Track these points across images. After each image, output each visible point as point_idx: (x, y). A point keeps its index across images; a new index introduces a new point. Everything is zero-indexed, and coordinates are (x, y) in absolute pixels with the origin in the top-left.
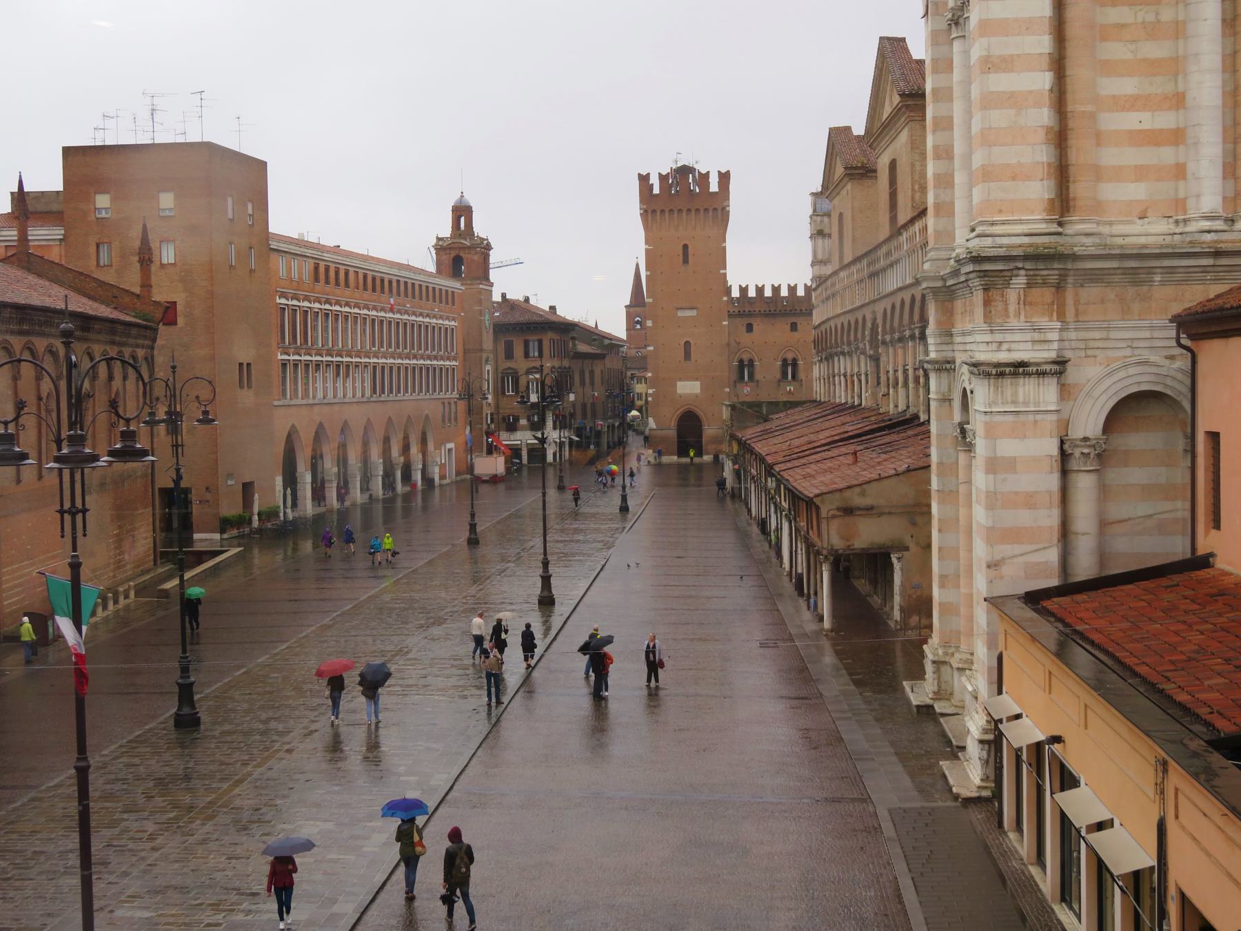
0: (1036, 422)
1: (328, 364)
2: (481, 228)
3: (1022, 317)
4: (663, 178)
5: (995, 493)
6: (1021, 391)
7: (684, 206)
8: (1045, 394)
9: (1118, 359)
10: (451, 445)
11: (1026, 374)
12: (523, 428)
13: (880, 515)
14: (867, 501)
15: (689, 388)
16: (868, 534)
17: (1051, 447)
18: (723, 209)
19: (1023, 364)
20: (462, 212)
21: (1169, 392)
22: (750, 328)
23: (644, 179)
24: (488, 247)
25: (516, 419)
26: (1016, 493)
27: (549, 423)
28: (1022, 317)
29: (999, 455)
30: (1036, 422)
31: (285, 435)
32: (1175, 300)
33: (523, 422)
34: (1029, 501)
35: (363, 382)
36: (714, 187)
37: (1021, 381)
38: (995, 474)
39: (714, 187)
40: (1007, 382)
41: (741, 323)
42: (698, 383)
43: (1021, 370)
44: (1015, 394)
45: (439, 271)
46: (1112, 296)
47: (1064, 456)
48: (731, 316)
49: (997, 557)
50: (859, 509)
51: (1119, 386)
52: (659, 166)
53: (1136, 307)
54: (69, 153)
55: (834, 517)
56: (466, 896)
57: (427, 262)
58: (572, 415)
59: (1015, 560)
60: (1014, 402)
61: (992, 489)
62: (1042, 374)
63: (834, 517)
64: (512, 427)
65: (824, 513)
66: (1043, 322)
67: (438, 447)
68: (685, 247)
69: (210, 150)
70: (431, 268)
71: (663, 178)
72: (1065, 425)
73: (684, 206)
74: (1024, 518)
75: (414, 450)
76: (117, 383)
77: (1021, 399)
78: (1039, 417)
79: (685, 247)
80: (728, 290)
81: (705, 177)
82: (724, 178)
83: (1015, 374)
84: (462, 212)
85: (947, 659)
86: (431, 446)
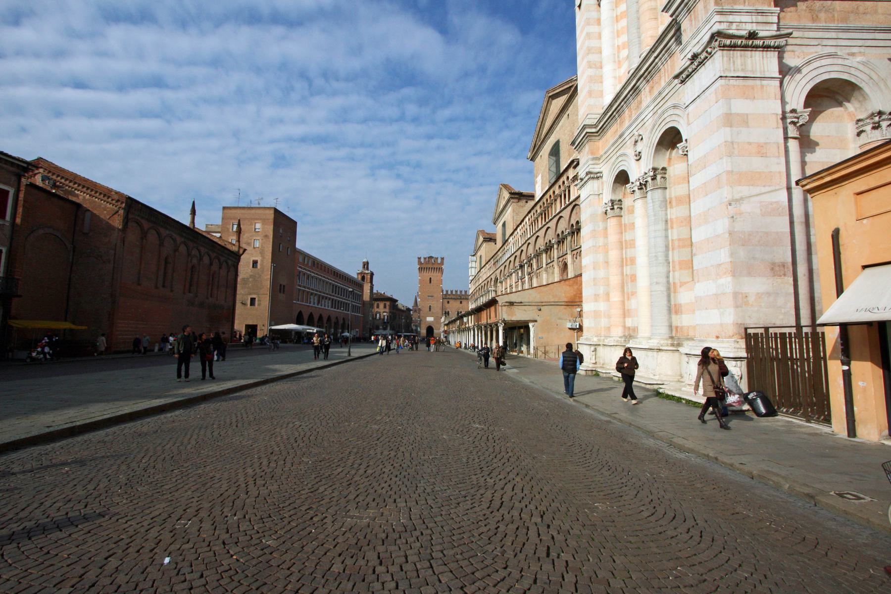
4: (425, 258)
5: (732, 143)
6: (749, 61)
8: (768, 63)
9: (812, 53)
15: (430, 319)
16: (518, 315)
20: (366, 265)
21: (853, 80)
23: (419, 258)
29: (733, 111)
30: (762, 86)
32: (852, 12)
34: (761, 150)
38: (731, 127)
41: (446, 301)
44: (744, 64)
46: (804, 8)
49: (737, 196)
51: (815, 73)
53: (822, 15)
56: (713, 381)
59: (752, 199)
61: (729, 139)
62: (766, 48)
71: (425, 258)
73: (430, 266)
74: (757, 164)
76: (215, 267)
77: (749, 67)
78: (765, 82)
82: (442, 259)
84: (366, 265)
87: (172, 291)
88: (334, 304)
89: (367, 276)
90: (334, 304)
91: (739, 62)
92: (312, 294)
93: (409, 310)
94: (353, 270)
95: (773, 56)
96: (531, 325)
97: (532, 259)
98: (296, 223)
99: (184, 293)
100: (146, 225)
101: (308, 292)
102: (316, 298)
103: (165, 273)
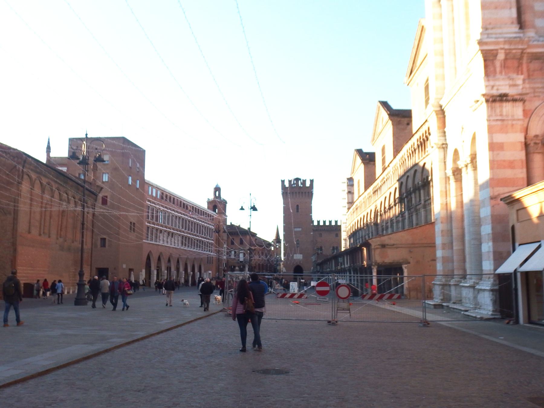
0: (513, 125)
1: (165, 231)
2: (223, 196)
3: (503, 73)
7: (297, 195)
8: (517, 110)
10: (210, 272)
11: (507, 101)
12: (237, 270)
13: (397, 248)
14: (392, 242)
16: (391, 256)
17: (521, 138)
18: (309, 192)
19: (506, 95)
22: (321, 235)
23: (283, 182)
24: (226, 202)
25: (235, 267)
26: (504, 161)
27: (247, 269)
28: (503, 73)
30: (513, 125)
31: (147, 255)
33: (237, 268)
34: (511, 165)
35: (178, 241)
36: (308, 184)
37: (504, 104)
39: (308, 184)
40: (497, 104)
42: (301, 255)
43: (505, 98)
44: (501, 111)
45: (208, 208)
47: (526, 145)
48: (314, 231)
49: (496, 194)
50: (388, 245)
52: (289, 177)
54: (72, 141)
55: (377, 248)
57: (204, 205)
58: (255, 267)
60: (501, 115)
62: (514, 100)
63: (377, 248)
64: (233, 270)
65: (373, 247)
66: (514, 76)
67: (205, 271)
68: (298, 206)
69: (124, 140)
70: (206, 208)
71: (290, 181)
72: (526, 131)
73: (297, 195)
75: (196, 270)
77: (504, 113)
78: (514, 122)
79: (298, 206)
80: (313, 222)
81: (304, 181)
82: (312, 181)
83: (501, 101)
85: (447, 283)
86: (203, 271)
87: (49, 237)
88: (186, 241)
89: (218, 204)
90: (186, 241)
91: (498, 111)
92: (161, 231)
93: (269, 245)
94: (201, 199)
95: (520, 105)
96: (404, 266)
97: (411, 194)
98: (144, 151)
99: (57, 239)
100: (34, 176)
101: (157, 229)
102: (180, 238)
103: (45, 219)
